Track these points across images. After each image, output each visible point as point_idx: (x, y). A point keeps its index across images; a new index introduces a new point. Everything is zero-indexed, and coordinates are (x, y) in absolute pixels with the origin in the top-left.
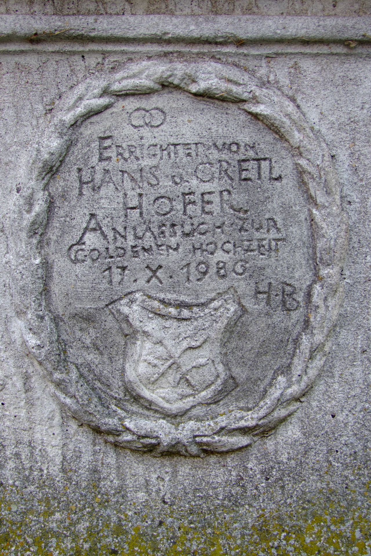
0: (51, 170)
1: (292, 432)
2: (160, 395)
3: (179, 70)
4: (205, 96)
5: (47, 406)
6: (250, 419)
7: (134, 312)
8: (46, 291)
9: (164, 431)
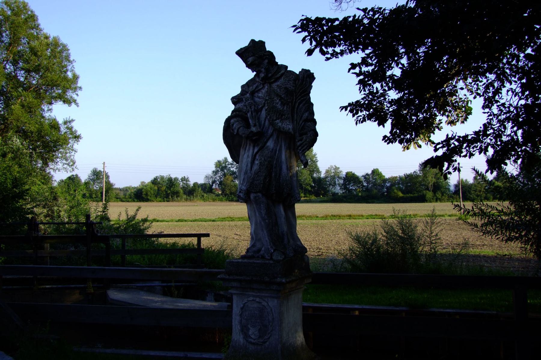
0: (242, 308)
1: (268, 343)
2: (253, 336)
3: (255, 299)
4: (257, 302)
5: (242, 336)
6: (262, 341)
7: (249, 326)
8: (241, 323)
9: (252, 341)
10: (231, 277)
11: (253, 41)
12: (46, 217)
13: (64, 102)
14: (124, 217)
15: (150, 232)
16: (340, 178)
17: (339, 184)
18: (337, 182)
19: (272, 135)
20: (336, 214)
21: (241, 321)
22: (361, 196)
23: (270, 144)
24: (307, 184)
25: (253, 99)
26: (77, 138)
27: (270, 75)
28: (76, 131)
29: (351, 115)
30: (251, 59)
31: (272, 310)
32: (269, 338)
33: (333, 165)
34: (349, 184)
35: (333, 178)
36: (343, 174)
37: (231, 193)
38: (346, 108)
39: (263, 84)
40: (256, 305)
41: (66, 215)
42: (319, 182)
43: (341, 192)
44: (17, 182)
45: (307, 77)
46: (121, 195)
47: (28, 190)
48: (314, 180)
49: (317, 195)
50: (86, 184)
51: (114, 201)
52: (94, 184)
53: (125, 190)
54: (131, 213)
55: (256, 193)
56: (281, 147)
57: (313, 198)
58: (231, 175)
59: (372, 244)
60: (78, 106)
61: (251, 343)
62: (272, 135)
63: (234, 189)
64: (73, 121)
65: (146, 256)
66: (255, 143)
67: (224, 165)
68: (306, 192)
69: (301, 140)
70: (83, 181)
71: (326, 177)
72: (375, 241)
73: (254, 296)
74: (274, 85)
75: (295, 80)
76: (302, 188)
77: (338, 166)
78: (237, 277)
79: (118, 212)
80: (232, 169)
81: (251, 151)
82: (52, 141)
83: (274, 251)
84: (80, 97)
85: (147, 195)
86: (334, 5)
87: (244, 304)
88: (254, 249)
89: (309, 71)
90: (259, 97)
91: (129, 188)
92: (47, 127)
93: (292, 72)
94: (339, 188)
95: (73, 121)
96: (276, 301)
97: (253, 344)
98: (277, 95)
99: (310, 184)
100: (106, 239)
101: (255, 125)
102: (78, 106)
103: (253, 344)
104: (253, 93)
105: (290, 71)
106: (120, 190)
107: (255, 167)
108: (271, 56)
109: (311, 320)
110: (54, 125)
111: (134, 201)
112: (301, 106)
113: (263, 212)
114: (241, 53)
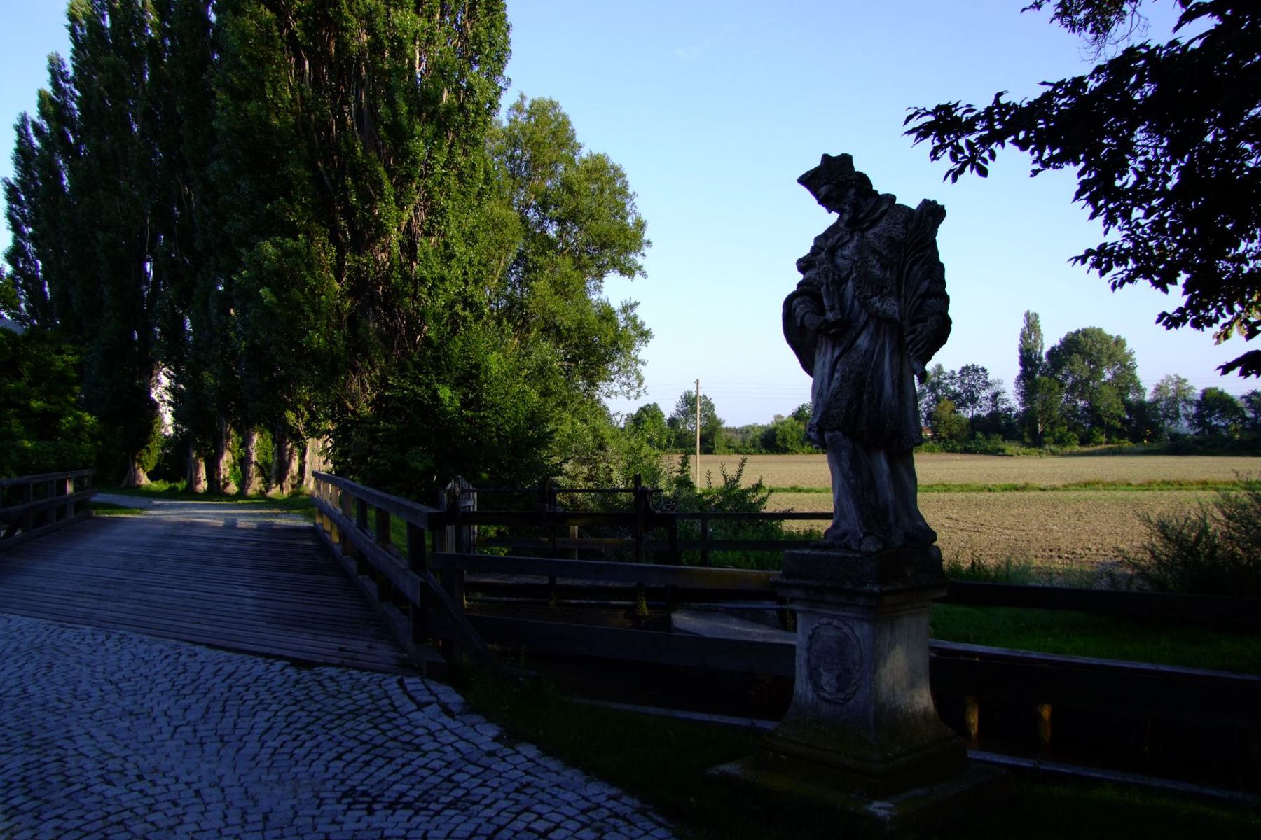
1: (852, 702)
2: (827, 688)
9: (827, 696)
10: (791, 581)
11: (826, 157)
12: (587, 480)
13: (623, 272)
14: (718, 482)
15: (770, 507)
16: (1190, 402)
17: (1187, 416)
18: (1181, 411)
19: (866, 324)
20: (1173, 479)
21: (809, 659)
22: (1240, 441)
23: (863, 341)
24: (1113, 417)
25: (832, 261)
26: (645, 335)
27: (862, 215)
28: (642, 324)
29: (1096, 272)
30: (823, 190)
31: (859, 642)
32: (854, 693)
33: (1172, 374)
34: (1210, 415)
35: (1173, 401)
36: (1197, 393)
37: (951, 437)
38: (1083, 259)
39: (852, 234)
40: (832, 633)
41: (621, 477)
42: (1140, 410)
43: (1192, 432)
44: (535, 419)
45: (933, 213)
46: (737, 442)
47: (552, 432)
48: (1129, 407)
49: (1136, 438)
50: (673, 422)
51: (724, 453)
52: (687, 421)
53: (746, 431)
54: (732, 471)
55: (832, 430)
56: (884, 343)
57: (1127, 444)
58: (950, 399)
59: (1198, 539)
60: (645, 277)
61: (824, 699)
62: (866, 324)
63: (956, 427)
64: (636, 304)
65: (751, 554)
66: (835, 340)
67: (935, 379)
68: (1110, 432)
69: (912, 333)
70: (667, 416)
71: (1157, 401)
72: (1204, 531)
73: (830, 616)
74: (869, 234)
75: (906, 222)
76: (1101, 425)
77: (1183, 377)
78: (798, 581)
79: (708, 474)
80: (952, 388)
81: (829, 355)
82: (601, 345)
83: (866, 535)
84: (645, 259)
85: (784, 440)
86: (1090, 51)
87: (814, 631)
88: (837, 532)
89: (935, 202)
90: (844, 257)
91: (753, 428)
92: (592, 318)
93: (903, 208)
94: (1186, 424)
95: (636, 304)
96: (866, 626)
97: (828, 701)
98: (875, 252)
99: (1119, 416)
100: (667, 520)
101: (832, 309)
102: (645, 277)
103: (828, 701)
104: (832, 251)
105: (899, 205)
106: (736, 431)
107: (835, 384)
108: (863, 180)
109: (945, 672)
110: (607, 316)
111: (760, 453)
112: (915, 268)
113: (846, 465)
114: (808, 180)
